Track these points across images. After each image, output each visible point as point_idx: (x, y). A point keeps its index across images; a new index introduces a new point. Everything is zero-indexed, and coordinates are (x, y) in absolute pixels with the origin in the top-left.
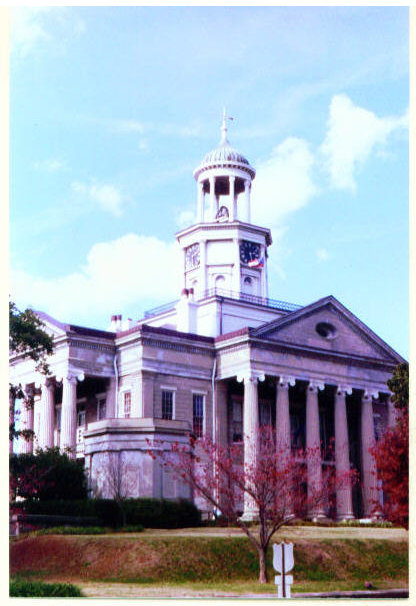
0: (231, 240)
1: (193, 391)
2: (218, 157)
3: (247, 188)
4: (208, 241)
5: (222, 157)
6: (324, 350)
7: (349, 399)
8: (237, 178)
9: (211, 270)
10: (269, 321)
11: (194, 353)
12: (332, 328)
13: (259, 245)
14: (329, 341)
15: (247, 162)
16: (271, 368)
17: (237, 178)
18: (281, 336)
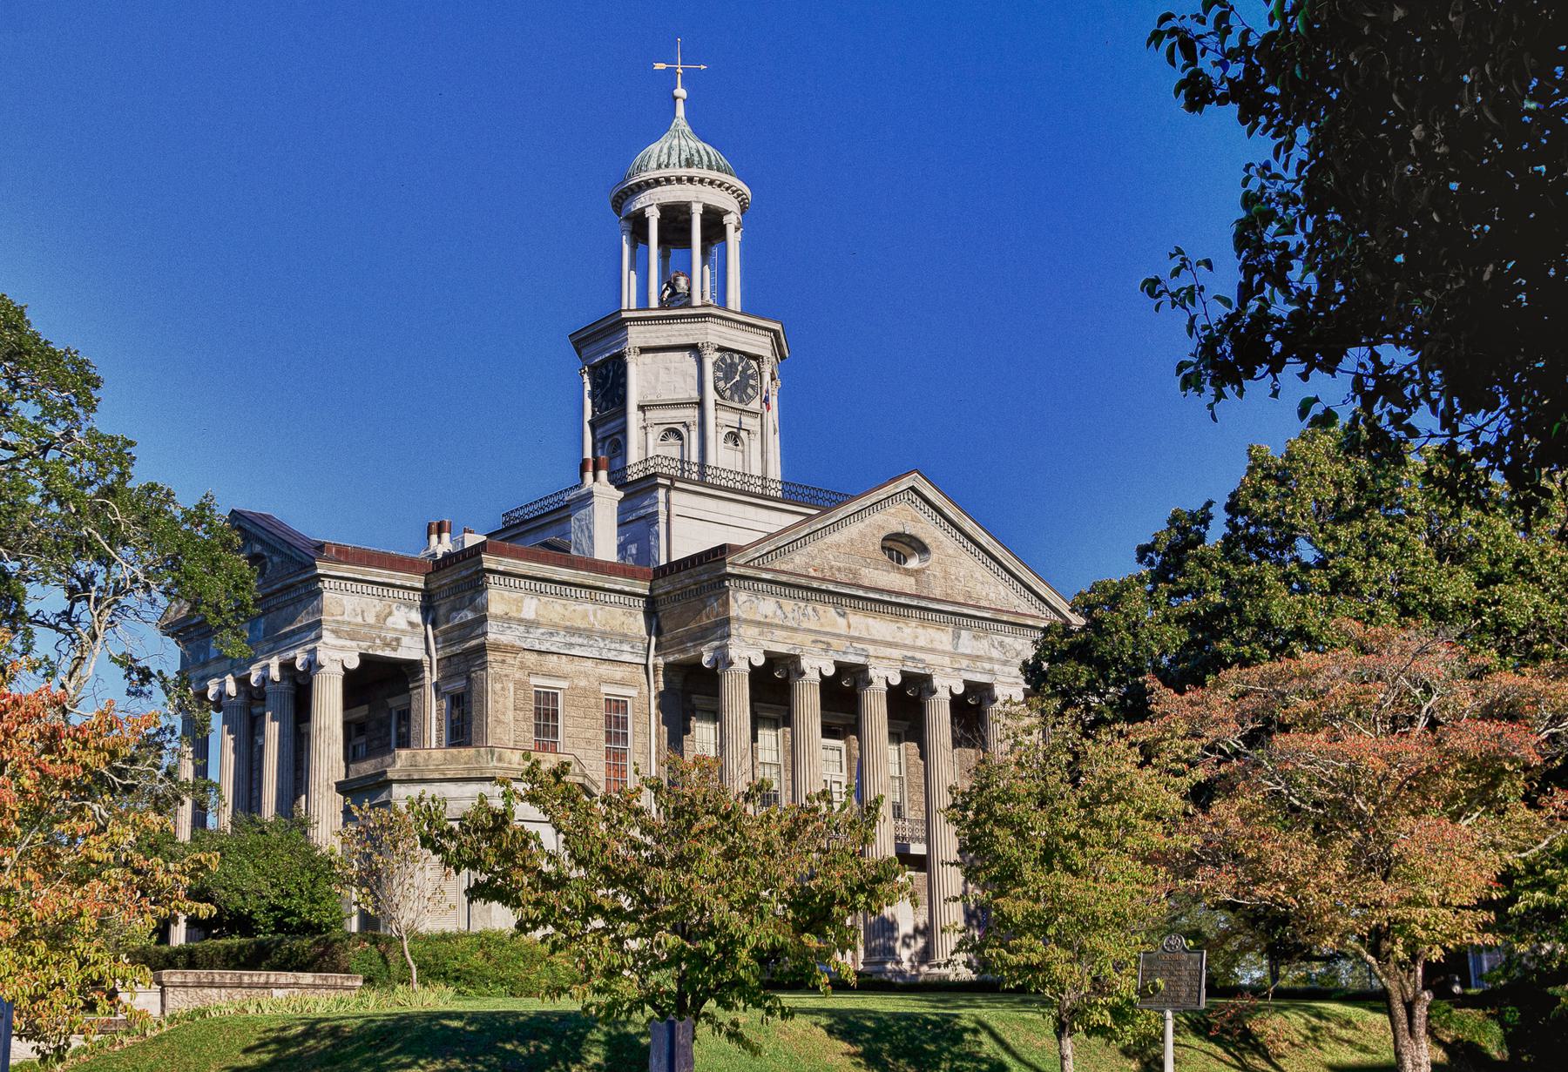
1: (605, 689)
2: (664, 158)
5: (674, 159)
6: (890, 592)
7: (957, 703)
9: (653, 415)
12: (921, 548)
14: (908, 572)
16: (779, 633)
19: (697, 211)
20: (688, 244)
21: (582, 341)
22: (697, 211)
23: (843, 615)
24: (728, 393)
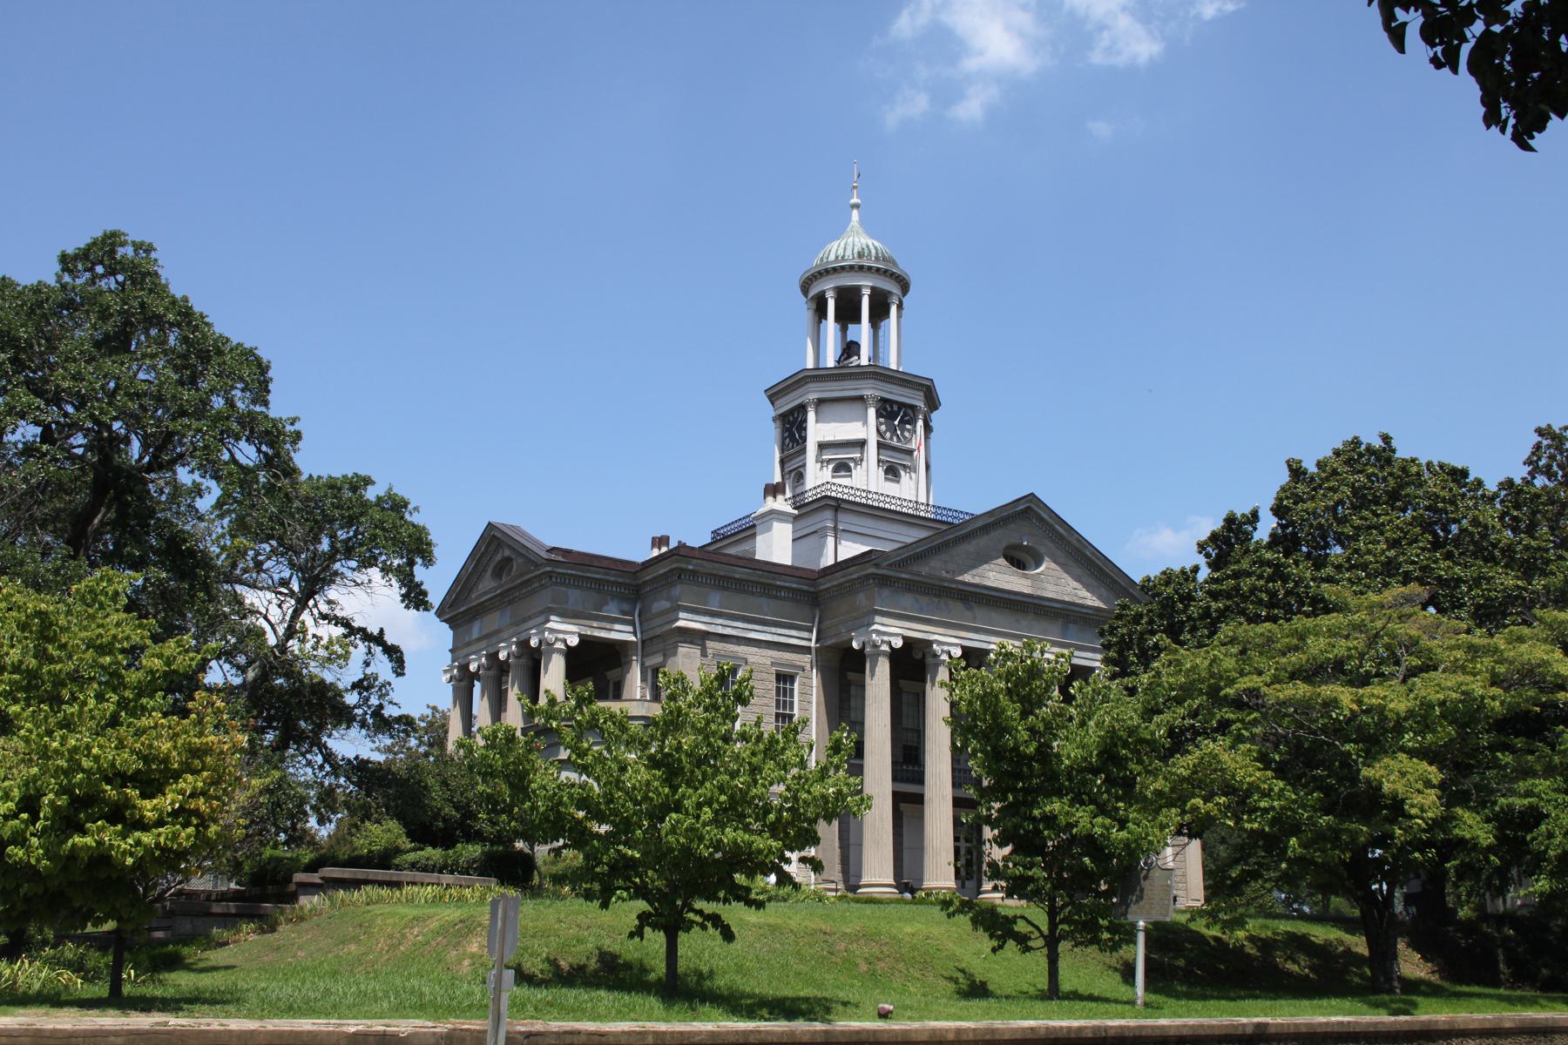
0: (861, 398)
2: (841, 252)
3: (894, 309)
4: (820, 402)
10: (909, 540)
11: (776, 597)
13: (913, 407)
14: (1026, 576)
15: (895, 264)
17: (873, 289)
18: (934, 568)
19: (866, 292)
20: (858, 320)
21: (774, 394)
22: (866, 292)
23: (970, 609)
24: (888, 435)
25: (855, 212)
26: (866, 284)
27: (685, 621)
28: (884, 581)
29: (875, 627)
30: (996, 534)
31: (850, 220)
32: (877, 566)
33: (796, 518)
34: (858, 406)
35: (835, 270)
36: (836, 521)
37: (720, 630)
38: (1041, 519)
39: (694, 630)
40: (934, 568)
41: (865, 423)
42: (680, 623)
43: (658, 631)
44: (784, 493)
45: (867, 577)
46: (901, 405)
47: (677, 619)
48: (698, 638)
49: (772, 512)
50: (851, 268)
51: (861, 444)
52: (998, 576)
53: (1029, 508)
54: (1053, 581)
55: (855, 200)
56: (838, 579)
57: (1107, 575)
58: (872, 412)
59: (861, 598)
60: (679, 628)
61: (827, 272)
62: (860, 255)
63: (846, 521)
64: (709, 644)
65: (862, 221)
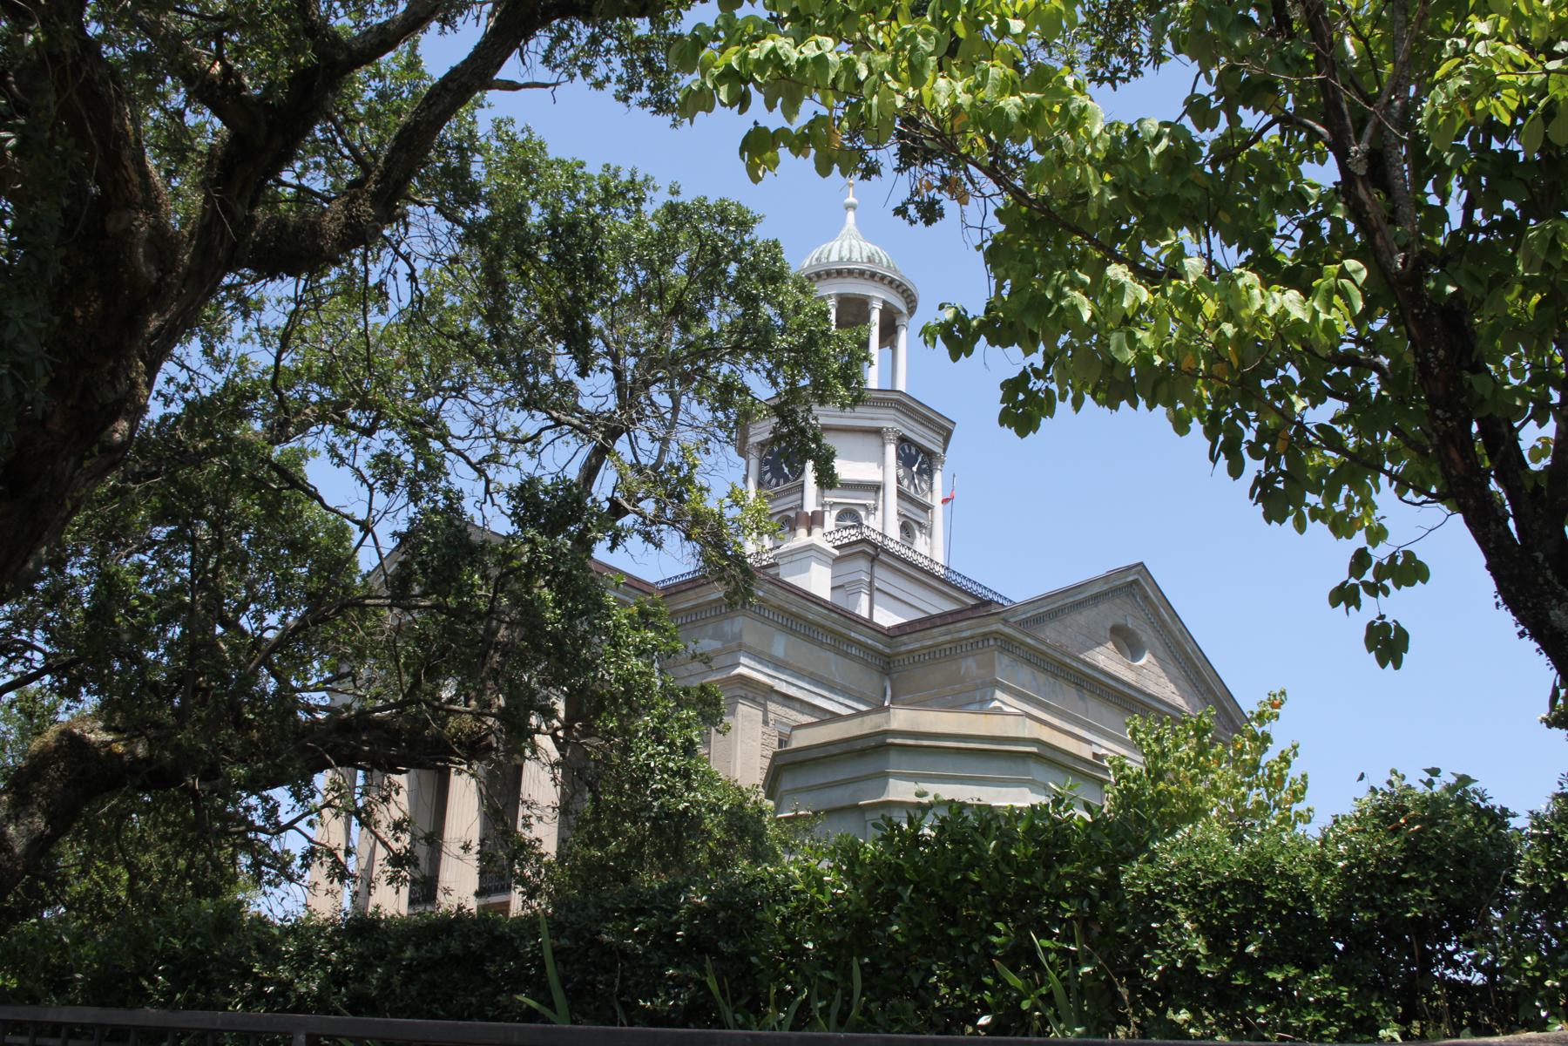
0: (877, 432)
8: (885, 302)
10: (934, 611)
11: (846, 655)
23: (1082, 698)
25: (851, 215)
26: (878, 296)
27: (747, 668)
28: (1007, 645)
29: (996, 704)
30: (1104, 607)
31: (843, 223)
32: (1005, 621)
33: (837, 560)
34: (873, 442)
35: (839, 273)
36: (872, 575)
37: (792, 691)
38: (1146, 597)
39: (758, 682)
40: (1051, 634)
41: (882, 463)
42: (741, 670)
43: (903, 649)
44: (822, 524)
45: (986, 636)
46: (921, 449)
47: (738, 664)
48: (761, 694)
49: (811, 548)
50: (862, 273)
51: (876, 488)
52: (1106, 658)
53: (1135, 582)
54: (1149, 675)
55: (851, 200)
56: (912, 644)
57: (1203, 681)
58: (891, 450)
59: (970, 666)
60: (741, 677)
61: (829, 274)
62: (870, 260)
63: (884, 578)
64: (771, 706)
65: (858, 223)
